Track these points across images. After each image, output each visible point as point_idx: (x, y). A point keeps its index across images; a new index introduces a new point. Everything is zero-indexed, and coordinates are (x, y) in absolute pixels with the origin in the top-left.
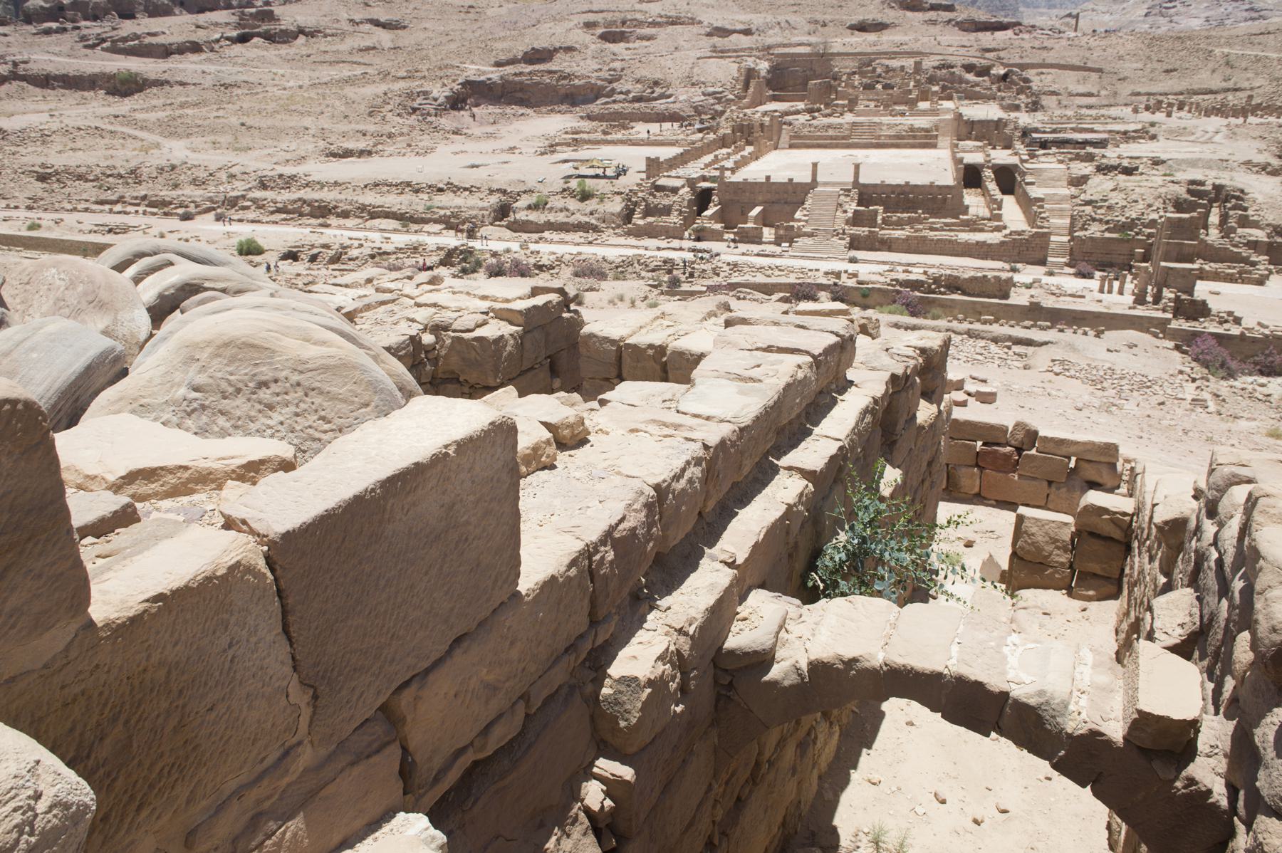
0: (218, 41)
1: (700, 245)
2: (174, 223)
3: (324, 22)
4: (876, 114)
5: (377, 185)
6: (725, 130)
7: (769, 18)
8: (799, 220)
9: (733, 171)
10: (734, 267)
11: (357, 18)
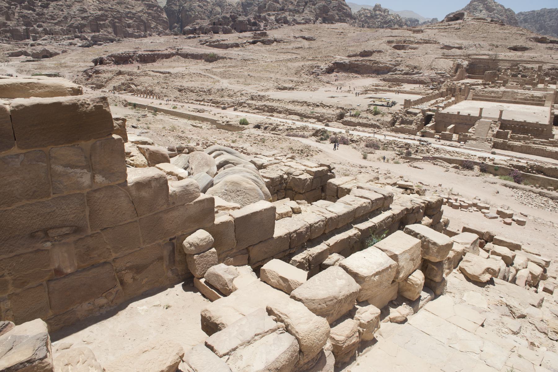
0: (245, 43)
1: (423, 139)
2: (220, 110)
3: (284, 37)
4: (516, 88)
5: (293, 102)
6: (443, 89)
7: (471, 42)
8: (471, 133)
9: (443, 108)
10: (437, 150)
11: (297, 36)
